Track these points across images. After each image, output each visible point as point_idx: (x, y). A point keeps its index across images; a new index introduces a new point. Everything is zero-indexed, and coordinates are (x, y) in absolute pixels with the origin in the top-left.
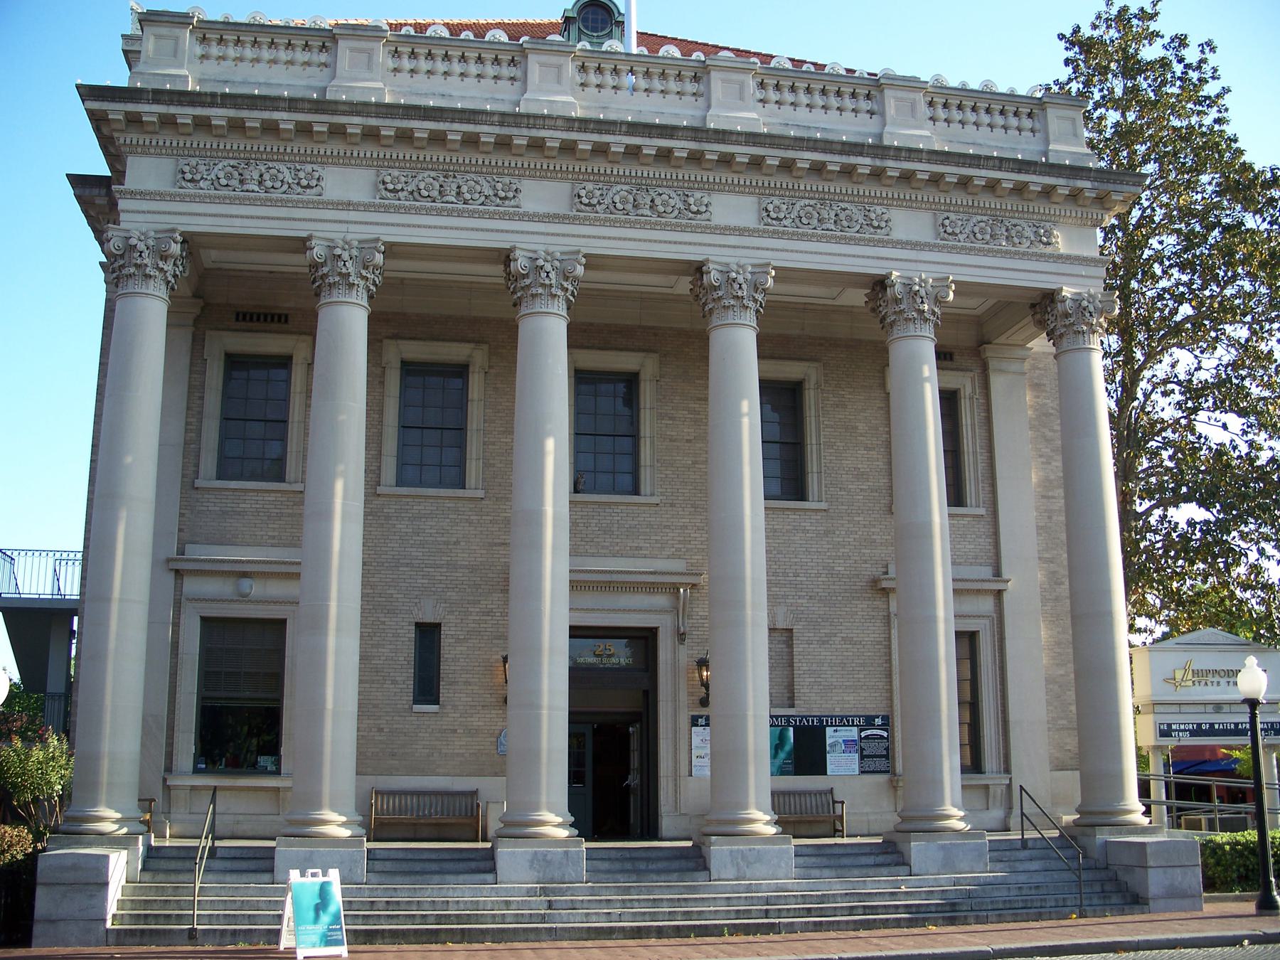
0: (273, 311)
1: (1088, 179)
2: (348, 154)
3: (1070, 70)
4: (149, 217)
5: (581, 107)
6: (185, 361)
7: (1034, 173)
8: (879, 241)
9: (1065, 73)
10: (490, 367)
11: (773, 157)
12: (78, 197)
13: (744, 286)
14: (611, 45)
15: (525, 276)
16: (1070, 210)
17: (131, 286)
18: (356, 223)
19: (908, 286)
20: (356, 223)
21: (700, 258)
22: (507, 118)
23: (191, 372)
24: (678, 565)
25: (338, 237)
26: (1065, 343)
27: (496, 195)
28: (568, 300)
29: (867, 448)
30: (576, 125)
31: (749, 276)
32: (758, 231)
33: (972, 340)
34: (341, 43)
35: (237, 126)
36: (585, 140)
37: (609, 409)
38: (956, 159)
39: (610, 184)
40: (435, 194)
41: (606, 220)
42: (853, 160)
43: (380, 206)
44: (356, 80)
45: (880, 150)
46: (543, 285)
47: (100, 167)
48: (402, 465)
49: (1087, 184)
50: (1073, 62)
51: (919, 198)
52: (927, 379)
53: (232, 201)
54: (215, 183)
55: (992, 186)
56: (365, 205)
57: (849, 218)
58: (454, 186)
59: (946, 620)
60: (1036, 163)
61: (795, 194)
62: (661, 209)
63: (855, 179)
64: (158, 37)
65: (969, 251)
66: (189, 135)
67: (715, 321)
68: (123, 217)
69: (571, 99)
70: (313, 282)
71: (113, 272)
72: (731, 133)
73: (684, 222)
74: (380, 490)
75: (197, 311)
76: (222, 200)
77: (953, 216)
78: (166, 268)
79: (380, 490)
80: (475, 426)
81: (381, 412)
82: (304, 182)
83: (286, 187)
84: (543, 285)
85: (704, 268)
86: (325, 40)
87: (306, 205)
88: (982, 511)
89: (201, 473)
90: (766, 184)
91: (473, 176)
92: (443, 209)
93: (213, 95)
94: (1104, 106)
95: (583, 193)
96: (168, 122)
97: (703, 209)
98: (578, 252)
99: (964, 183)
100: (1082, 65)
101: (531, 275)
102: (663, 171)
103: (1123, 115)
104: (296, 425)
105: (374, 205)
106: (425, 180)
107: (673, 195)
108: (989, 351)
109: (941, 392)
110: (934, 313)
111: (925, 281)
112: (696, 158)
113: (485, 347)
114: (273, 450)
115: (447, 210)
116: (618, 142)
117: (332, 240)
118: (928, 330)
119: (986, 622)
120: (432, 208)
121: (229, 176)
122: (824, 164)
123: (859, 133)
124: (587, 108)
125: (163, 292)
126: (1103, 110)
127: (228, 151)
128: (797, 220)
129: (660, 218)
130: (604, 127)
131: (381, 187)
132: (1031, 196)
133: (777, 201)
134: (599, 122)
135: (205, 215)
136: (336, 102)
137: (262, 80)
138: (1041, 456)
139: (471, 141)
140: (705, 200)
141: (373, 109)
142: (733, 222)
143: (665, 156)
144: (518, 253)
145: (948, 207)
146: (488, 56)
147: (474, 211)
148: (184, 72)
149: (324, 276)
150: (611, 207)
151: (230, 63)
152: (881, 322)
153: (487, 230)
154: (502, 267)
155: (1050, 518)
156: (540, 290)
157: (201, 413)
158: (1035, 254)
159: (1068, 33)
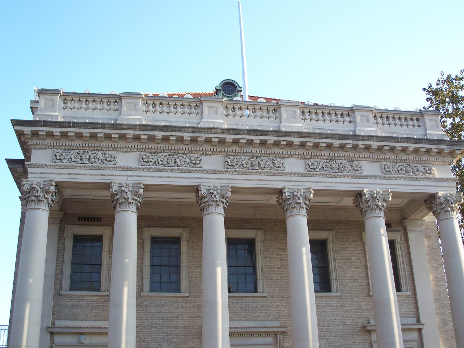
0: (94, 216)
1: (445, 145)
2: (127, 147)
3: (429, 103)
4: (41, 175)
5: (227, 124)
6: (56, 238)
7: (422, 143)
8: (358, 176)
9: (427, 104)
10: (190, 238)
11: (310, 142)
12: (10, 169)
13: (301, 198)
14: (238, 98)
15: (205, 197)
16: (438, 158)
17: (33, 205)
18: (131, 176)
19: (371, 195)
20: (131, 176)
21: (281, 187)
22: (195, 130)
23: (58, 243)
24: (277, 324)
25: (123, 182)
26: (441, 216)
27: (191, 163)
28: (224, 207)
29: (357, 268)
30: (225, 131)
31: (303, 194)
32: (305, 174)
33: (400, 218)
34: (123, 100)
35: (79, 136)
36: (229, 138)
37: (242, 254)
38: (388, 139)
39: (241, 156)
40: (165, 163)
41: (239, 172)
42: (344, 142)
43: (141, 168)
44: (130, 115)
45: (355, 137)
46: (213, 201)
47: (20, 155)
48: (152, 282)
49: (445, 147)
50: (430, 99)
51: (374, 157)
52: (383, 235)
53: (77, 168)
54: (70, 160)
55: (404, 150)
56: (135, 168)
57: (344, 167)
58: (173, 159)
59: (400, 343)
60: (422, 139)
61: (320, 158)
62: (263, 166)
63: (345, 150)
64: (46, 100)
65: (397, 178)
66: (59, 140)
67: (289, 214)
68: (30, 175)
69: (222, 121)
70: (113, 202)
71: (25, 199)
72: (292, 132)
73: (273, 171)
74: (143, 294)
75: (61, 217)
76: (73, 168)
77: (388, 164)
78: (48, 197)
79: (143, 294)
80: (184, 265)
81: (143, 260)
82: (108, 159)
83: (100, 161)
84: (213, 201)
85: (283, 191)
86: (117, 99)
87: (109, 169)
88: (409, 293)
89: (63, 288)
90: (308, 154)
91: (181, 155)
92: (168, 169)
93: (69, 123)
94: (445, 117)
95: (229, 160)
96: (50, 135)
97: (281, 165)
98: (228, 186)
99: (392, 149)
100: (434, 100)
101: (208, 197)
102: (263, 150)
103: (454, 120)
104: (105, 266)
105: (139, 168)
106: (161, 157)
107: (268, 160)
108: (407, 222)
109: (389, 241)
110: (383, 206)
111: (379, 192)
112: (277, 144)
113: (188, 230)
114: (95, 277)
115: (171, 169)
116: (243, 138)
117: (121, 184)
118: (381, 214)
119: (415, 343)
120: (163, 169)
121: (76, 157)
122: (332, 144)
123: (346, 131)
124: (229, 124)
125: (47, 207)
126: (444, 119)
127: (75, 147)
128: (322, 169)
129: (262, 170)
130: (237, 132)
131: (142, 160)
132: (421, 153)
133: (312, 161)
134: (235, 130)
135: (65, 174)
136: (122, 125)
137: (90, 117)
138: (433, 267)
139: (180, 140)
140: (282, 162)
141: (138, 127)
142: (294, 171)
143: (263, 143)
144: (202, 187)
145: (386, 160)
146: (186, 104)
147: (182, 170)
148: (56, 114)
149: (117, 200)
150: (241, 166)
151: (76, 110)
152: (360, 211)
153: (188, 178)
154: (195, 194)
155: (439, 294)
156: (212, 203)
157: (63, 261)
158: (425, 178)
159: (427, 87)
